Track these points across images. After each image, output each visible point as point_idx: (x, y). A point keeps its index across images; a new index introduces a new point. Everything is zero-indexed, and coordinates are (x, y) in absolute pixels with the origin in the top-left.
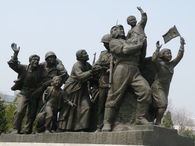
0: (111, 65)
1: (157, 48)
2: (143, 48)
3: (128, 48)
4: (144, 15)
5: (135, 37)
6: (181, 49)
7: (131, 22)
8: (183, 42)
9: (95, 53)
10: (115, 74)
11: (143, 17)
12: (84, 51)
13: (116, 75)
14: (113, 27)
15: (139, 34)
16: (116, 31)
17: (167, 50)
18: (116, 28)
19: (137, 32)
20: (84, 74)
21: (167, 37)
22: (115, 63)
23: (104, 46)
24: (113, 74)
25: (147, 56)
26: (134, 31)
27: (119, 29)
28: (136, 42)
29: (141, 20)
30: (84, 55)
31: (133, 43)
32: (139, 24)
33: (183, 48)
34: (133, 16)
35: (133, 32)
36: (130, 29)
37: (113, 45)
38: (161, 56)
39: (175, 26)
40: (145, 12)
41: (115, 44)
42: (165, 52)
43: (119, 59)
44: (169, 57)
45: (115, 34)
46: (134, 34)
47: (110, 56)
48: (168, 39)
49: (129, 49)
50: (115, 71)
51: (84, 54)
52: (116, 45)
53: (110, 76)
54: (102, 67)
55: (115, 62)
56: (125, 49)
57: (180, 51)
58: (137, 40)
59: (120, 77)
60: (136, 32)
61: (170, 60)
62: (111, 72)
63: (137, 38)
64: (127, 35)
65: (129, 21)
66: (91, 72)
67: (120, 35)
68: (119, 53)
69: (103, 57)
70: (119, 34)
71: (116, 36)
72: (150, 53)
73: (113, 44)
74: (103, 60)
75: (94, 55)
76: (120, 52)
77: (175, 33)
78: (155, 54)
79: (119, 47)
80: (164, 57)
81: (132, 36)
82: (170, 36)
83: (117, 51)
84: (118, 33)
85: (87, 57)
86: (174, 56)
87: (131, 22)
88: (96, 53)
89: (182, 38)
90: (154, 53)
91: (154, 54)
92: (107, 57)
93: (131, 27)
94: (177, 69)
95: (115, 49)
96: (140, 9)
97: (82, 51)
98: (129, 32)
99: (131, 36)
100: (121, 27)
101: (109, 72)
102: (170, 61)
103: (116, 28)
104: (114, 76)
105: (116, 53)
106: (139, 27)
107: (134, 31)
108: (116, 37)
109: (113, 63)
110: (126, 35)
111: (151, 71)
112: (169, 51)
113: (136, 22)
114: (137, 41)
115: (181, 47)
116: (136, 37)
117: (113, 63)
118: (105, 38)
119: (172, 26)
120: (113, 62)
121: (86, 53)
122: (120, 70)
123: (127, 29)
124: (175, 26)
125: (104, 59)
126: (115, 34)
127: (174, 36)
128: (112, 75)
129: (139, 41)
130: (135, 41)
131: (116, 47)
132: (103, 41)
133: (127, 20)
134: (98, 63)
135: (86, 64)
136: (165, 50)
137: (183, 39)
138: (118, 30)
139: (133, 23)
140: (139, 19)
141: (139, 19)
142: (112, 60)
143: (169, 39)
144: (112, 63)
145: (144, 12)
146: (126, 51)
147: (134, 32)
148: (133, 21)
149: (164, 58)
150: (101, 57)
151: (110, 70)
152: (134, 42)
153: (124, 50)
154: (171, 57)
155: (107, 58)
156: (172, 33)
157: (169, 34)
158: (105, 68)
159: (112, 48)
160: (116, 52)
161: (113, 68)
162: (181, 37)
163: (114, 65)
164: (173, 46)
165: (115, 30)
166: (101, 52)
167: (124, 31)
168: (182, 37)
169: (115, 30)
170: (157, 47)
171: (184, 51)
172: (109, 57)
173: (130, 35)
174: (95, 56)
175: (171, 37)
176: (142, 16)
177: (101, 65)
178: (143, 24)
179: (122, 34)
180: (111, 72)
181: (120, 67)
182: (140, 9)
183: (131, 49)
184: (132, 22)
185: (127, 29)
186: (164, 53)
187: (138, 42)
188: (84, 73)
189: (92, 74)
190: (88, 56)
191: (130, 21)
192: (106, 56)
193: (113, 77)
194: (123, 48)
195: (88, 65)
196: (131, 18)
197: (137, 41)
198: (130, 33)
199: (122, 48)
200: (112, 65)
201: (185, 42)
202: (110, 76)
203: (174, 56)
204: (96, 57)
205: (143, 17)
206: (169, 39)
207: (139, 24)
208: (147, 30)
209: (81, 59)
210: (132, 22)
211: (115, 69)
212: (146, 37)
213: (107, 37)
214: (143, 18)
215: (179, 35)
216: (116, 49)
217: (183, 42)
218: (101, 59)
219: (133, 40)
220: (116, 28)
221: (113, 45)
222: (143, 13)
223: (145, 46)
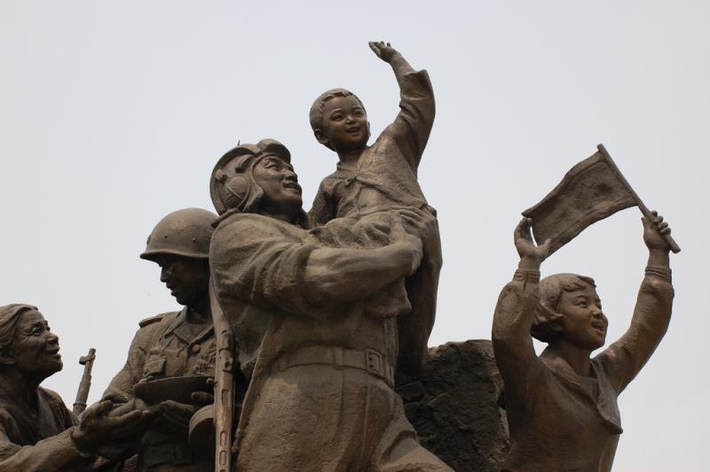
0: (222, 380)
1: (518, 259)
2: (419, 278)
3: (343, 259)
4: (417, 87)
5: (369, 212)
6: (655, 282)
7: (339, 123)
8: (660, 241)
9: (86, 354)
10: (251, 432)
11: (412, 99)
12: (29, 313)
13: (260, 437)
14: (225, 157)
15: (392, 193)
16: (249, 173)
17: (577, 280)
18: (246, 157)
19: (379, 180)
20: (23, 458)
21: (549, 222)
22: (250, 367)
23: (163, 280)
24: (243, 436)
25: (437, 338)
26: (359, 178)
27: (264, 161)
28: (380, 235)
29: (400, 117)
30: (32, 339)
31: (366, 236)
32: (383, 139)
33: (666, 276)
34: (351, 94)
35: (353, 181)
36: (333, 169)
37: (238, 250)
38: (543, 319)
39: (601, 148)
40: (416, 66)
41: (248, 242)
42: (567, 295)
43: (277, 335)
44: (594, 325)
45: (245, 195)
46: (359, 194)
47: (200, 342)
48: (565, 227)
49: (349, 268)
50: (250, 410)
51: (30, 333)
52: (258, 245)
53: (219, 449)
54: (156, 408)
55: (244, 362)
56: (320, 262)
57: (646, 290)
58: (387, 225)
59: (289, 448)
60: (370, 181)
61: (601, 344)
62: (221, 424)
63: (388, 213)
64: (313, 208)
65: (327, 116)
66: (75, 440)
67: (277, 197)
68: (286, 290)
69: (156, 353)
70: (270, 192)
71: (249, 203)
72: (464, 313)
73: (241, 239)
74: (158, 368)
75: (82, 363)
76: (286, 282)
77: (604, 190)
78: (512, 296)
79: (278, 254)
80: (560, 321)
81: (350, 204)
82: (578, 208)
83: (269, 276)
84: (264, 182)
85: (49, 348)
86: (619, 321)
87: (339, 123)
88: (93, 351)
89: (655, 214)
90: (508, 289)
91: (503, 296)
92: (182, 345)
93: (339, 160)
94: (633, 404)
95: (254, 268)
96: (386, 54)
97: (16, 310)
98: (329, 189)
99: (340, 207)
100: (279, 154)
101: (209, 425)
102: (594, 354)
103: (248, 161)
104: (245, 444)
105: (259, 294)
106: (387, 152)
107: (361, 175)
108: (255, 203)
109: (236, 365)
110: (307, 206)
111: (464, 427)
112: (584, 288)
113: (364, 129)
114: (387, 230)
115: (649, 271)
116: (375, 208)
117: (236, 365)
118: (173, 227)
119: (587, 152)
120: (231, 360)
121: (42, 326)
122: (291, 403)
123: (315, 167)
124: (601, 148)
125: (165, 362)
126: (244, 194)
127: (602, 206)
128: (233, 439)
129: (398, 230)
130: (377, 227)
131: (261, 257)
132: (156, 247)
133: (312, 113)
134: (118, 391)
135: (40, 398)
136: (567, 281)
137: (661, 219)
138: (260, 169)
139: (349, 131)
140: (382, 109)
141: (382, 109)
142: (227, 349)
143: (571, 230)
144: (227, 364)
145: (412, 69)
146: (330, 279)
147: (358, 186)
148: (350, 118)
149: (559, 329)
150: (140, 351)
151: (218, 412)
152: (369, 232)
153: (316, 271)
154: (601, 323)
155: (185, 353)
156: (592, 189)
157: (568, 201)
158: (176, 409)
159: (227, 267)
160: (261, 284)
161: (238, 398)
162: (644, 210)
163: (240, 380)
164: (606, 258)
165: (240, 170)
166: (143, 325)
167: (294, 178)
168: (651, 208)
169: (240, 170)
170: (521, 255)
171: (671, 293)
172: (196, 348)
173: (331, 202)
174: (88, 370)
175: (579, 215)
176: (405, 90)
177: (140, 393)
178: (413, 133)
179: (288, 193)
180: (221, 424)
181: (278, 394)
182: (386, 54)
183: (360, 264)
184: (338, 123)
185: (315, 167)
186: (556, 301)
187: (394, 233)
188: (27, 451)
189: (82, 454)
190: (55, 341)
191: (334, 119)
192: (175, 342)
193: (238, 452)
194: (310, 261)
195: (53, 408)
196: (336, 100)
197: (387, 230)
198: (335, 188)
199: (303, 260)
200: (230, 377)
201: (675, 236)
202: (222, 447)
203: (619, 321)
204: (92, 374)
205: (412, 99)
206: (571, 230)
207: (383, 139)
208: (435, 175)
209: (10, 362)
210: (338, 123)
211: (255, 397)
212: (434, 213)
213: (183, 225)
214: (409, 103)
215: (633, 200)
216: (264, 269)
217: (660, 241)
218: (141, 365)
219: (364, 221)
220: (246, 157)
221: (236, 245)
222: (408, 73)
223: (432, 261)
